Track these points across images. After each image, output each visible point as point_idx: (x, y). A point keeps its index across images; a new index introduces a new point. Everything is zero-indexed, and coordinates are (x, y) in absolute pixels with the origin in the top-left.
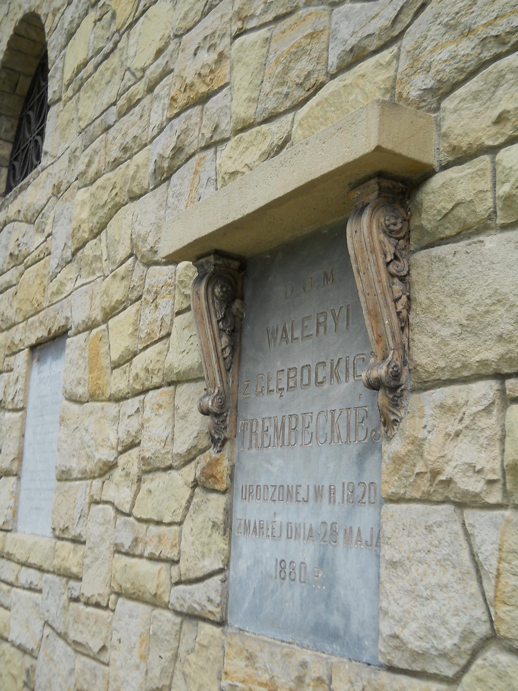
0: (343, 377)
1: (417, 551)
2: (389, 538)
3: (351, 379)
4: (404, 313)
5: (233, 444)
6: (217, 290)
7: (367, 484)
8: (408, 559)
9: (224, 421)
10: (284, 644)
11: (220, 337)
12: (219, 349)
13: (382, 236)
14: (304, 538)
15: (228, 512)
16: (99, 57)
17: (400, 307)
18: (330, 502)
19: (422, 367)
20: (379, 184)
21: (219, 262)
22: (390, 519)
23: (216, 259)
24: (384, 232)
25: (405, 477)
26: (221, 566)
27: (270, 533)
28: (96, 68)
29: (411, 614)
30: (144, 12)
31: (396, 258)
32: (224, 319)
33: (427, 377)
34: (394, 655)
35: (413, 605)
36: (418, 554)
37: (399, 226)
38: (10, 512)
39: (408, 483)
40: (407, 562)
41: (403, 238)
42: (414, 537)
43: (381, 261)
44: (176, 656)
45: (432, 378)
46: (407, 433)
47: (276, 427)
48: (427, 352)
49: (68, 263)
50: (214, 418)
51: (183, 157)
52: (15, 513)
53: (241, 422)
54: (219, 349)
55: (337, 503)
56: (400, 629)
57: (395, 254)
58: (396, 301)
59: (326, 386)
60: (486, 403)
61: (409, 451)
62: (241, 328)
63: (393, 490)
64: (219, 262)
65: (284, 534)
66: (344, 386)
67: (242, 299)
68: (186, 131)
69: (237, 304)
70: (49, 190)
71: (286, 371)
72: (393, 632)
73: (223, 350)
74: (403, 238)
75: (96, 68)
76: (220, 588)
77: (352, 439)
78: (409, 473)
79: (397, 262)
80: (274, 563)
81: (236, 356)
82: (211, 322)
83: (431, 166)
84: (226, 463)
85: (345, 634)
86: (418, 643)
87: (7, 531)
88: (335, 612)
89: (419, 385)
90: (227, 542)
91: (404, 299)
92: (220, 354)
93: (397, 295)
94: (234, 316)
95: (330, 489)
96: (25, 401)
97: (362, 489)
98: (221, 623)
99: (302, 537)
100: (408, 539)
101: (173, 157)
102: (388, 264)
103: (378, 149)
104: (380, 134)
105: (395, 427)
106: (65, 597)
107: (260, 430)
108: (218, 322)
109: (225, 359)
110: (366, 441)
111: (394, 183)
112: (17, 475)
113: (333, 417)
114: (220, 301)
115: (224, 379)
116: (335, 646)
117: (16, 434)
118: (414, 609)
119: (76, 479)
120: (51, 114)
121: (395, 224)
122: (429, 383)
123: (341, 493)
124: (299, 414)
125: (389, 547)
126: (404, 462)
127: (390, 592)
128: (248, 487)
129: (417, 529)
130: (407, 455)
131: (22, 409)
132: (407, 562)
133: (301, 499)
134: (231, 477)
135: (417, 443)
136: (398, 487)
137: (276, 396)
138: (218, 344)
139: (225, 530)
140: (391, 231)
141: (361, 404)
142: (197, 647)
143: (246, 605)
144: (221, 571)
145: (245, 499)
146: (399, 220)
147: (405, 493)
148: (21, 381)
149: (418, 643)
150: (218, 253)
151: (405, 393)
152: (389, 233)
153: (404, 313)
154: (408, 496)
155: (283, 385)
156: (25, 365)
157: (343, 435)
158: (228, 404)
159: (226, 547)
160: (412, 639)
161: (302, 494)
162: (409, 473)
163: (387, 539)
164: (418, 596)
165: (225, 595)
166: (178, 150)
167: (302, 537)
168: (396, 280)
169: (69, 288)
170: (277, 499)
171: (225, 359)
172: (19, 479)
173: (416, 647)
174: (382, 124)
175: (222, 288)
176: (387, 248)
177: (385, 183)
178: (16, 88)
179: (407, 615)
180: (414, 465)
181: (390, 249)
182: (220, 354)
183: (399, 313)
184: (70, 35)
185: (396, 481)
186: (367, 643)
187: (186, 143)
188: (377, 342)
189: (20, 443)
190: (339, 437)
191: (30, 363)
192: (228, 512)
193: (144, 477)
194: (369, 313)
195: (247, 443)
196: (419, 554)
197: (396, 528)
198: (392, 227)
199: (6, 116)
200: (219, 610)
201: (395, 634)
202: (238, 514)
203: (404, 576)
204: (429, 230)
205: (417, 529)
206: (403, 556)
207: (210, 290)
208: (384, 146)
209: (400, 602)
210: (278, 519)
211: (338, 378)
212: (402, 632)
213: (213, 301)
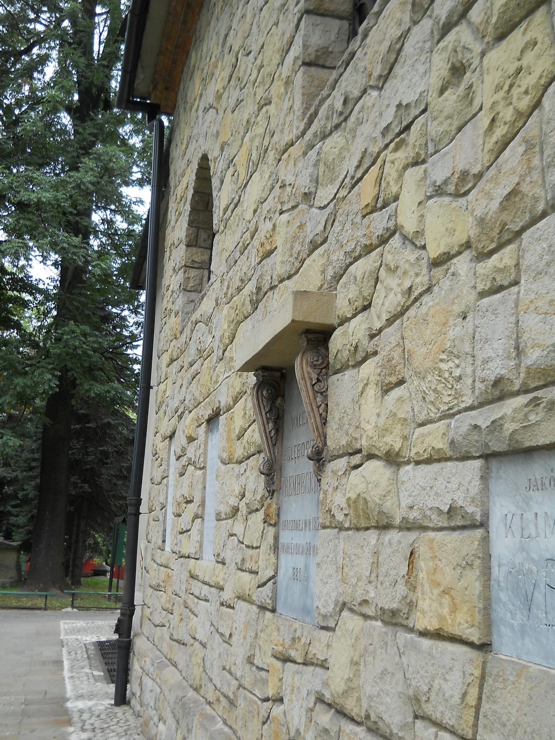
4: (324, 414)
5: (279, 493)
6: (265, 393)
9: (272, 479)
11: (268, 423)
12: (268, 431)
13: (309, 369)
15: (276, 538)
16: (232, 206)
17: (321, 411)
20: (306, 337)
21: (266, 374)
23: (262, 372)
24: (311, 366)
28: (232, 212)
30: (251, 176)
31: (318, 380)
32: (270, 411)
37: (320, 361)
38: (198, 544)
41: (324, 368)
43: (308, 384)
44: (257, 634)
49: (221, 360)
51: (262, 293)
52: (201, 546)
54: (268, 431)
57: (318, 379)
58: (319, 407)
60: (344, 470)
62: (283, 416)
64: (266, 374)
67: (283, 397)
68: (261, 276)
69: (279, 401)
70: (213, 303)
73: (270, 432)
74: (324, 368)
75: (232, 212)
76: (271, 588)
79: (320, 383)
81: (280, 435)
82: (261, 414)
83: (333, 325)
84: (274, 506)
87: (198, 559)
91: (323, 405)
92: (268, 434)
93: (319, 404)
94: (278, 409)
96: (205, 461)
98: (273, 611)
101: (257, 293)
102: (313, 385)
103: (293, 321)
104: (293, 313)
106: (218, 603)
108: (266, 413)
109: (272, 437)
111: (317, 335)
112: (202, 517)
114: (267, 400)
115: (272, 451)
117: (200, 487)
119: (224, 519)
120: (217, 237)
121: (318, 361)
131: (204, 468)
134: (278, 515)
138: (267, 428)
139: (274, 550)
140: (315, 365)
144: (274, 577)
146: (320, 358)
148: (202, 447)
150: (264, 368)
151: (326, 463)
152: (314, 366)
153: (324, 414)
155: (296, 456)
156: (204, 435)
158: (274, 467)
159: (275, 561)
165: (275, 592)
166: (259, 289)
168: (319, 394)
169: (220, 380)
171: (272, 437)
172: (203, 520)
174: (295, 305)
175: (267, 391)
176: (312, 376)
177: (310, 336)
178: (208, 206)
181: (314, 376)
182: (268, 434)
183: (321, 415)
184: (222, 182)
187: (262, 284)
189: (203, 493)
191: (207, 432)
192: (276, 538)
193: (249, 516)
198: (315, 363)
199: (203, 229)
200: (271, 602)
202: (282, 540)
207: (260, 393)
208: (297, 319)
213: (262, 400)
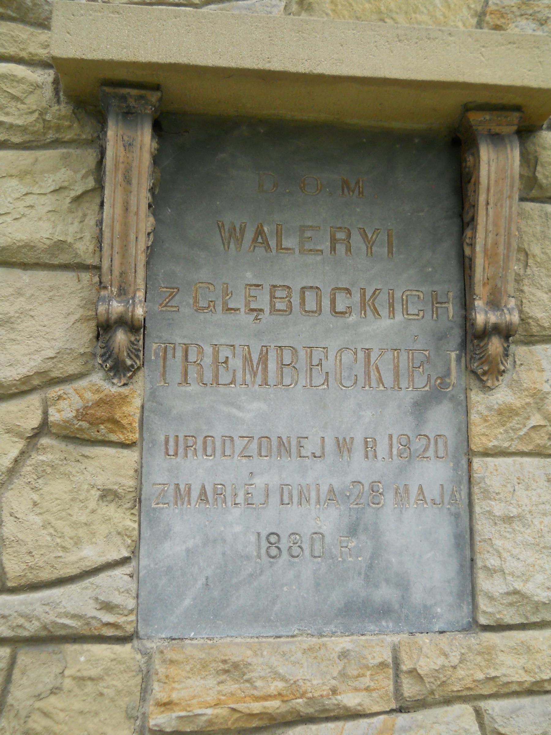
0: (384, 312)
1: (540, 504)
2: (498, 494)
3: (399, 317)
7: (432, 436)
8: (530, 512)
10: (282, 640)
14: (318, 502)
18: (367, 457)
19: (536, 320)
22: (495, 473)
25: (513, 430)
26: (126, 554)
27: (240, 499)
29: (536, 567)
33: (537, 332)
34: (505, 613)
35: (537, 557)
36: (542, 507)
39: (516, 436)
40: (528, 516)
42: (535, 490)
45: (544, 333)
46: (525, 385)
47: (247, 359)
48: (542, 307)
50: (130, 334)
53: (155, 346)
55: (379, 458)
56: (522, 584)
59: (353, 318)
61: (528, 404)
63: (495, 443)
65: (295, 499)
66: (385, 323)
71: (267, 288)
72: (512, 589)
77: (404, 384)
78: (519, 426)
80: (253, 538)
85: (402, 606)
86: (545, 594)
88: (384, 584)
89: (522, 337)
90: (136, 518)
95: (366, 443)
97: (424, 442)
99: (313, 500)
100: (527, 492)
105: (500, 378)
107: (208, 360)
110: (427, 388)
113: (368, 357)
116: (384, 623)
118: (539, 562)
122: (536, 338)
123: (387, 447)
124: (299, 348)
125: (497, 502)
126: (517, 414)
127: (504, 549)
128: (181, 439)
129: (537, 482)
130: (523, 407)
132: (528, 516)
133: (309, 454)
135: (540, 396)
136: (503, 441)
137: (248, 319)
141: (417, 346)
142: (68, 683)
143: (187, 602)
144: (124, 561)
145: (176, 454)
147: (510, 446)
149: (545, 594)
154: (512, 449)
157: (388, 379)
160: (539, 591)
161: (309, 448)
162: (519, 426)
163: (494, 495)
164: (544, 548)
167: (313, 500)
170: (255, 453)
173: (544, 598)
179: (531, 569)
180: (528, 418)
185: (501, 433)
186: (439, 610)
188: (484, 285)
190: (380, 380)
194: (485, 251)
195: (175, 376)
196: (543, 506)
197: (508, 483)
201: (515, 589)
203: (523, 530)
204: (544, 185)
205: (537, 482)
206: (523, 510)
209: (521, 557)
210: (258, 481)
211: (376, 312)
212: (524, 586)
